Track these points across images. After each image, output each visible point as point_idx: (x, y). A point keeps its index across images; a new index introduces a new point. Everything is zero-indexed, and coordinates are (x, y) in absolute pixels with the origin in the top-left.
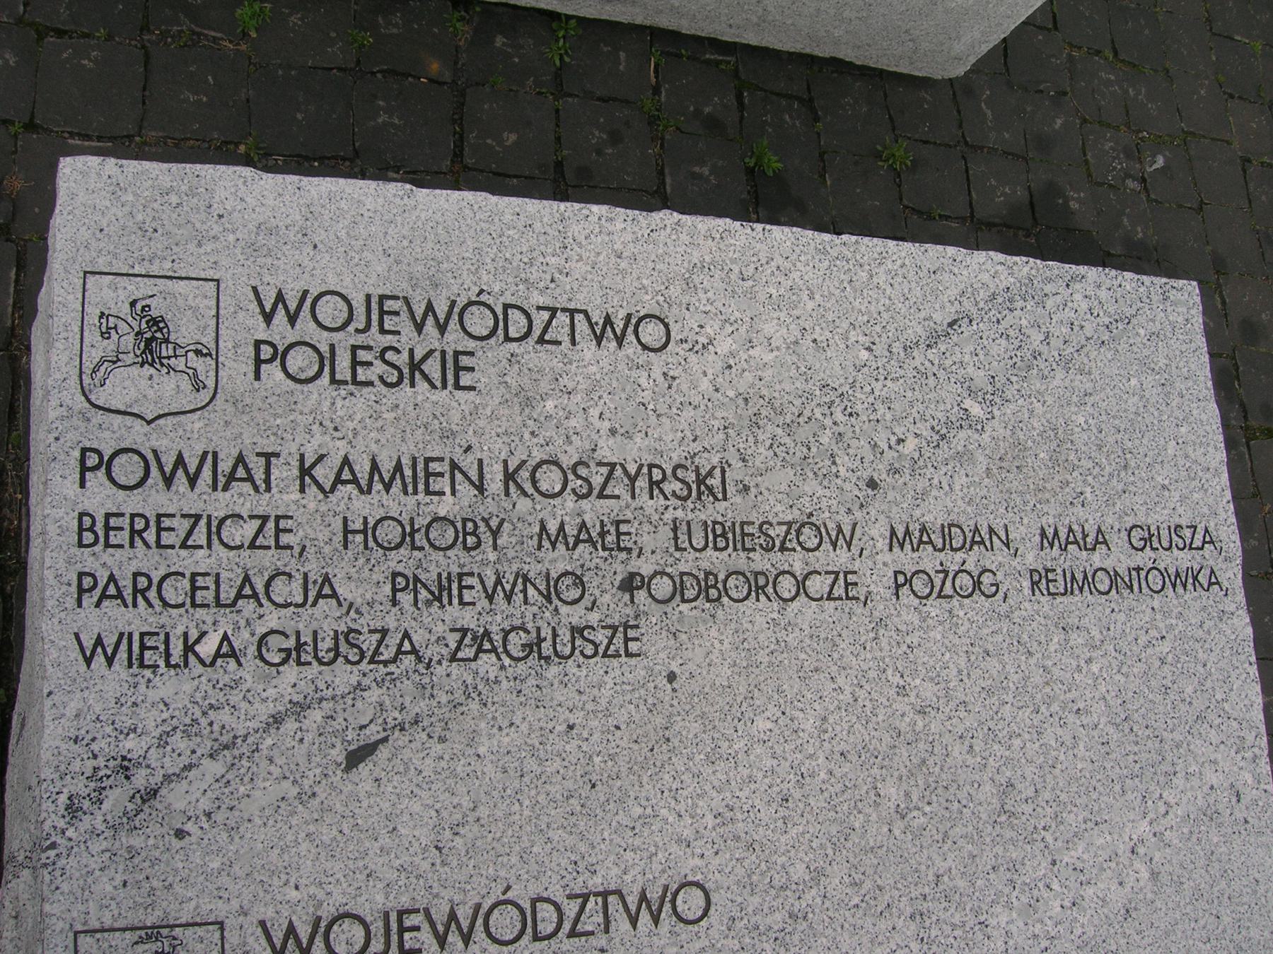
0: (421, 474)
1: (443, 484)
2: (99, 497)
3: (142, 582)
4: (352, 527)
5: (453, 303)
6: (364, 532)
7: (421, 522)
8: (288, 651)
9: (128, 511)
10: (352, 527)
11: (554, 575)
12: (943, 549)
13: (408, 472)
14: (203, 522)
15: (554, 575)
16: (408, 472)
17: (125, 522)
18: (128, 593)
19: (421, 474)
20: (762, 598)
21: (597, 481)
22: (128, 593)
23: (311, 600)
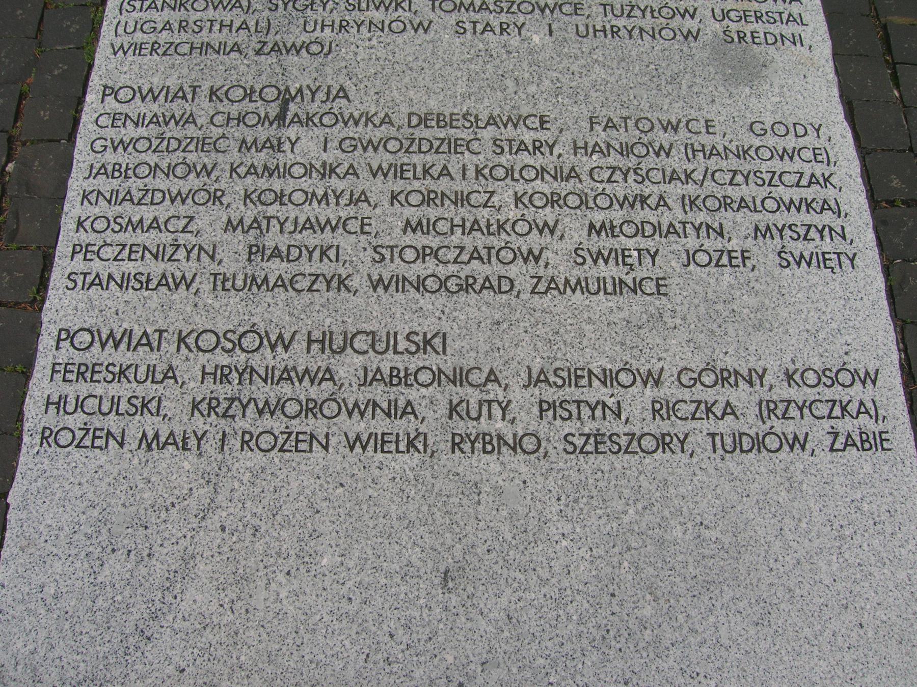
0: (573, 378)
1: (584, 382)
2: (66, 353)
3: (537, 144)
4: (207, 371)
5: (279, 400)
7: (258, 87)
9: (77, 361)
10: (207, 371)
11: (435, 384)
12: (597, 293)
13: (583, 284)
15: (435, 384)
16: (583, 284)
18: (531, 148)
19: (573, 378)
20: (726, 385)
21: (802, 233)
22: (531, 148)
23: (299, 229)
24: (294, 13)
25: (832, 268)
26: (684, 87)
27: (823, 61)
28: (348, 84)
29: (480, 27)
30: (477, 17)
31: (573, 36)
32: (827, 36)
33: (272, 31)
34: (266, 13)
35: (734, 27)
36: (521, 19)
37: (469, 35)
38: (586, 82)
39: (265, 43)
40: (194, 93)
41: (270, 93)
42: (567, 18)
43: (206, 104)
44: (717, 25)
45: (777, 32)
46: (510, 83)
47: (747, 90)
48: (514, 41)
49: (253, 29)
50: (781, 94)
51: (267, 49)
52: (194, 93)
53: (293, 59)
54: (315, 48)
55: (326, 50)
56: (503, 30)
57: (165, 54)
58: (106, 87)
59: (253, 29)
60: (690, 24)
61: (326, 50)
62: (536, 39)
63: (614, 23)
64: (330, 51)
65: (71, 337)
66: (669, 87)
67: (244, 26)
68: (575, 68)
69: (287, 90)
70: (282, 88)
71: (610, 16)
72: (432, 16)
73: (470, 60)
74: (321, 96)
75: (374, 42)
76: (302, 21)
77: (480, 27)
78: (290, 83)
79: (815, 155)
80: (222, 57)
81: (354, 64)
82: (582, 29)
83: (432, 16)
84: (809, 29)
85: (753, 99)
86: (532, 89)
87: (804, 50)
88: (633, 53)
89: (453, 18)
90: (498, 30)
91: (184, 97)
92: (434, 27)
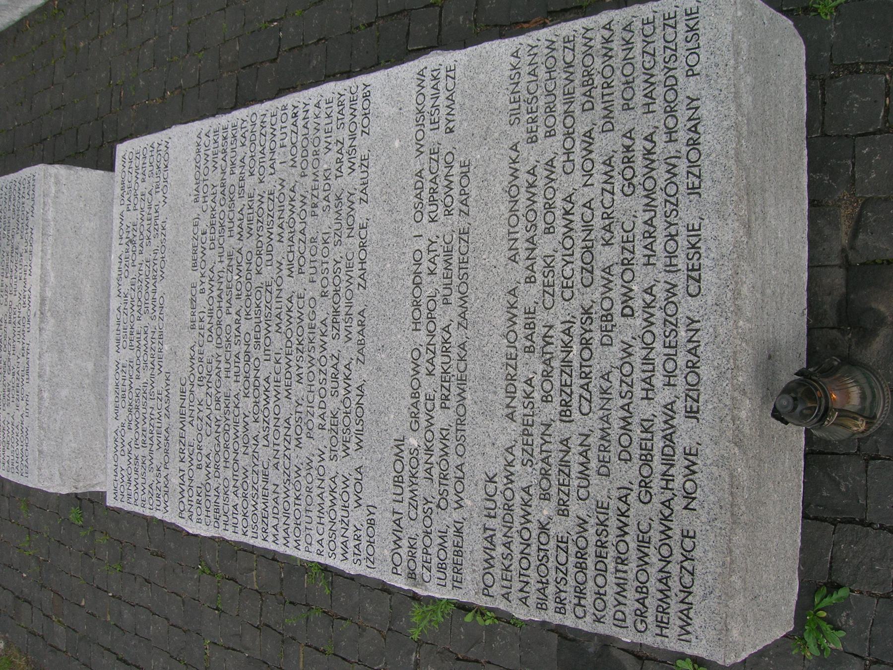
6: (670, 257)
8: (647, 491)
14: (561, 468)
17: (660, 614)
25: (613, 326)
33: (630, 486)
65: (487, 587)
79: (648, 23)
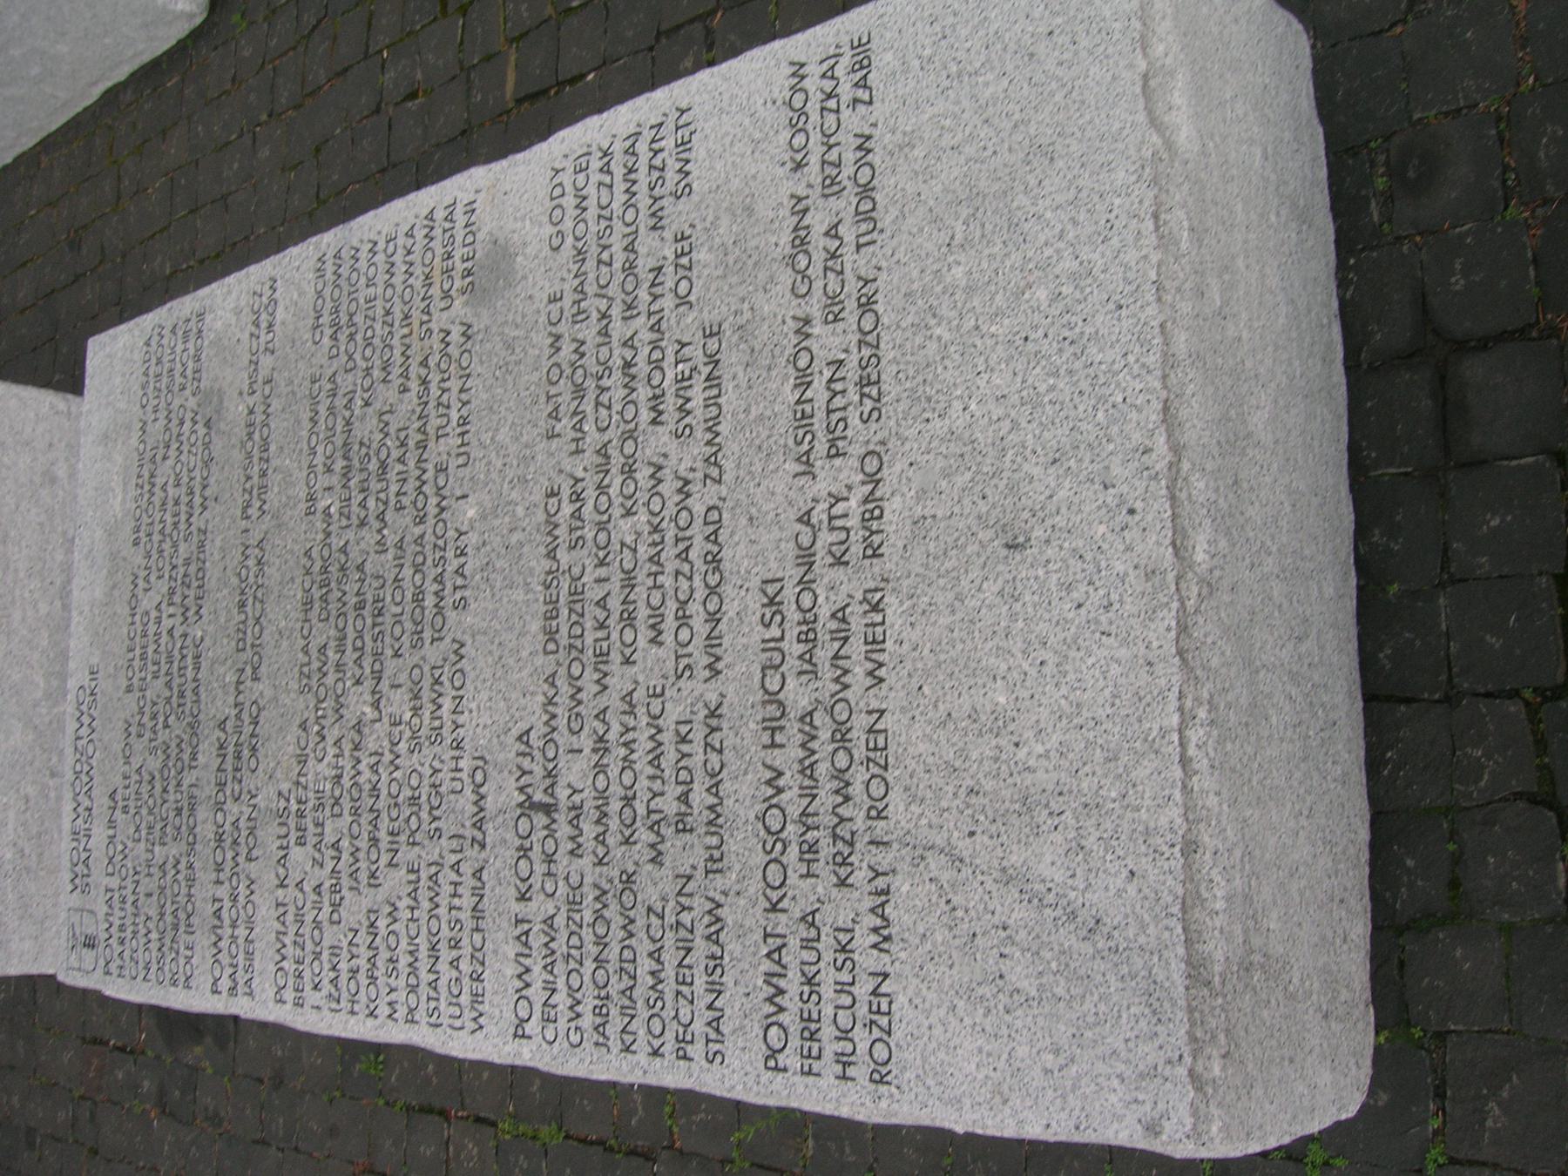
24: (443, 807)
26: (516, 333)
27: (491, 174)
28: (515, 732)
29: (460, 582)
30: (449, 586)
31: (468, 469)
32: (466, 174)
33: (461, 831)
34: (443, 841)
35: (458, 284)
36: (451, 534)
37: (467, 593)
38: (513, 449)
39: (473, 839)
40: (522, 921)
41: (524, 825)
42: (451, 480)
43: (533, 905)
44: (457, 302)
45: (462, 233)
46: (514, 538)
47: (519, 259)
48: (473, 539)
49: (459, 856)
50: (523, 219)
51: (479, 836)
52: (522, 921)
53: (489, 803)
54: (479, 777)
55: (481, 763)
56: (462, 554)
57: (483, 964)
58: (515, 1035)
59: (459, 856)
60: (456, 331)
61: (481, 763)
62: (471, 513)
63: (454, 423)
64: (482, 758)
66: (518, 350)
67: (456, 867)
68: (499, 464)
69: (520, 805)
70: (519, 812)
71: (448, 429)
72: (448, 640)
73: (492, 588)
74: (526, 763)
75: (473, 706)
76: (452, 797)
77: (460, 582)
78: (514, 803)
80: (487, 891)
81: (495, 727)
82: (461, 460)
83: (448, 640)
84: (460, 195)
85: (528, 250)
86: (520, 511)
87: (481, 197)
88: (485, 397)
89: (452, 615)
90: (462, 560)
91: (527, 933)
92: (459, 636)
